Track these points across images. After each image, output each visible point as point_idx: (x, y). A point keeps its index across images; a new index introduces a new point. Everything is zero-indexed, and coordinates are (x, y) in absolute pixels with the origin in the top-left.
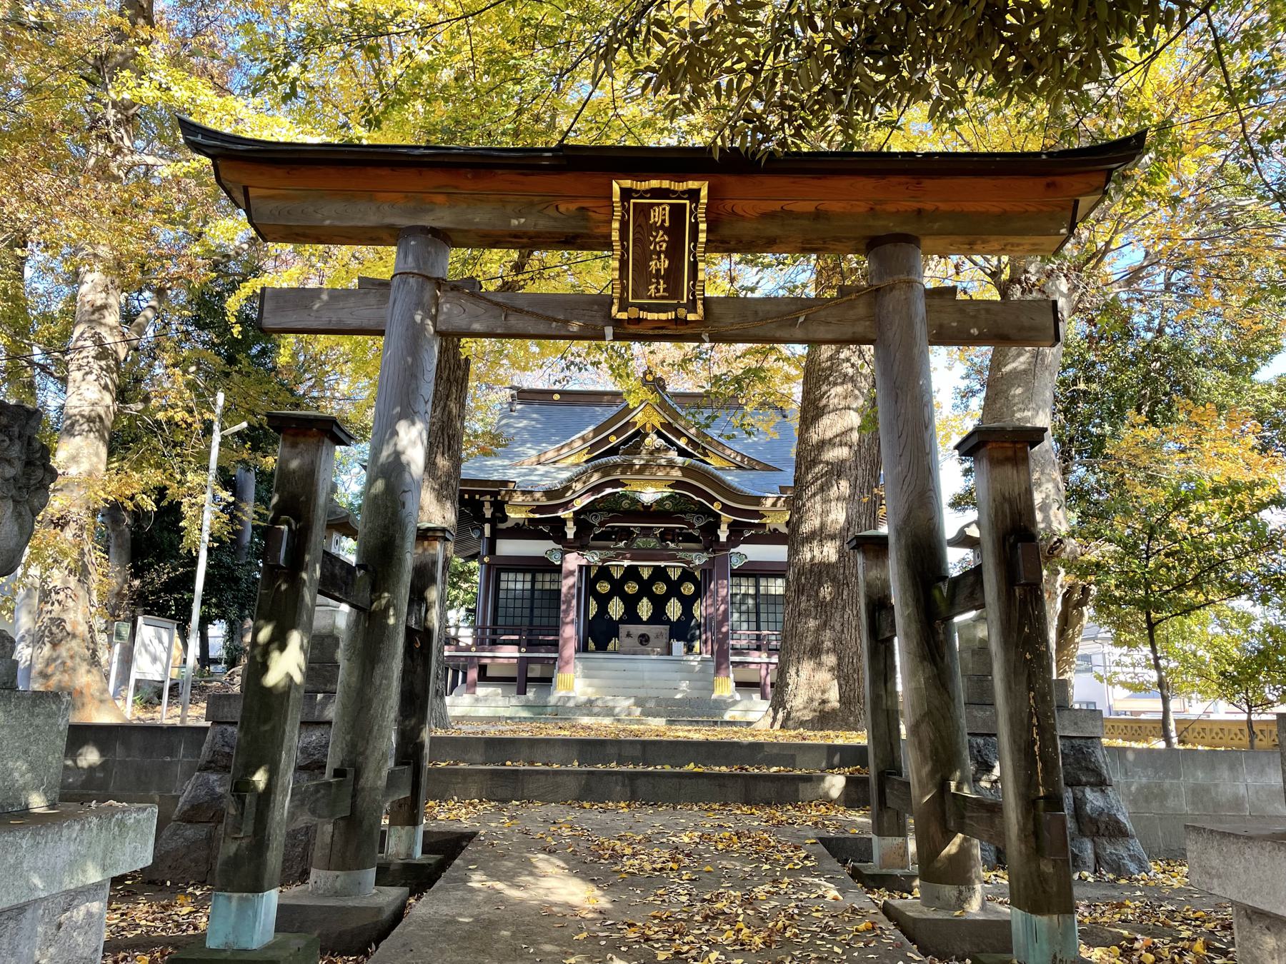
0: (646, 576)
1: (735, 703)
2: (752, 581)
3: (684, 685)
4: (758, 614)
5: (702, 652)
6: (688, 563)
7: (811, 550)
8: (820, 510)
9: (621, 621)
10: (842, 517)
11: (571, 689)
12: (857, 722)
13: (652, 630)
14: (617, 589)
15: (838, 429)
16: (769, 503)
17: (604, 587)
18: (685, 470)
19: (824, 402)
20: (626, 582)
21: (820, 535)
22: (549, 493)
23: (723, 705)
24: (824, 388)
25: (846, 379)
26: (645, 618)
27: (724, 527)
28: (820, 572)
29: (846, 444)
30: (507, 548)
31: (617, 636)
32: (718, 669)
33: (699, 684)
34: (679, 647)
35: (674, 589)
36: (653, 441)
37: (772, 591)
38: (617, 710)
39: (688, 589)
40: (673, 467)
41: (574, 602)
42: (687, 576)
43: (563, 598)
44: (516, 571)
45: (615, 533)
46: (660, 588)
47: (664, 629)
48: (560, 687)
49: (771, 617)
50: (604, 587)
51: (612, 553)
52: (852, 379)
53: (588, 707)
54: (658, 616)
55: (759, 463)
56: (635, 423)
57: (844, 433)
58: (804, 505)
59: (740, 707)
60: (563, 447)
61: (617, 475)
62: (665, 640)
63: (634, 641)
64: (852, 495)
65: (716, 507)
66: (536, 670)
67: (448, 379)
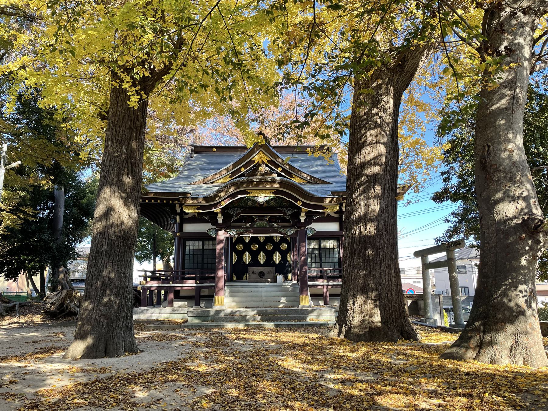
0: (262, 241)
1: (312, 311)
2: (317, 241)
3: (283, 300)
4: (320, 258)
5: (292, 281)
6: (284, 234)
7: (359, 228)
8: (363, 204)
9: (250, 265)
11: (222, 304)
12: (393, 335)
14: (247, 248)
15: (373, 154)
16: (328, 201)
17: (240, 247)
18: (281, 183)
19: (363, 140)
21: (365, 219)
22: (207, 199)
23: (305, 313)
25: (376, 125)
26: (262, 262)
27: (303, 214)
28: (365, 241)
29: (378, 164)
30: (189, 228)
31: (248, 272)
32: (301, 292)
33: (292, 298)
34: (280, 278)
35: (277, 247)
36: (263, 169)
38: (248, 317)
39: (284, 246)
40: (275, 182)
41: (223, 258)
42: (283, 240)
44: (194, 240)
46: (270, 247)
47: (271, 268)
48: (216, 304)
49: (328, 260)
50: (240, 247)
51: (243, 230)
52: (380, 126)
53: (231, 317)
54: (269, 262)
55: (319, 180)
56: (254, 161)
58: (353, 201)
59: (315, 313)
60: (216, 174)
61: (244, 188)
63: (256, 276)
64: (383, 194)
65: (299, 204)
66: (205, 292)
67: (130, 127)
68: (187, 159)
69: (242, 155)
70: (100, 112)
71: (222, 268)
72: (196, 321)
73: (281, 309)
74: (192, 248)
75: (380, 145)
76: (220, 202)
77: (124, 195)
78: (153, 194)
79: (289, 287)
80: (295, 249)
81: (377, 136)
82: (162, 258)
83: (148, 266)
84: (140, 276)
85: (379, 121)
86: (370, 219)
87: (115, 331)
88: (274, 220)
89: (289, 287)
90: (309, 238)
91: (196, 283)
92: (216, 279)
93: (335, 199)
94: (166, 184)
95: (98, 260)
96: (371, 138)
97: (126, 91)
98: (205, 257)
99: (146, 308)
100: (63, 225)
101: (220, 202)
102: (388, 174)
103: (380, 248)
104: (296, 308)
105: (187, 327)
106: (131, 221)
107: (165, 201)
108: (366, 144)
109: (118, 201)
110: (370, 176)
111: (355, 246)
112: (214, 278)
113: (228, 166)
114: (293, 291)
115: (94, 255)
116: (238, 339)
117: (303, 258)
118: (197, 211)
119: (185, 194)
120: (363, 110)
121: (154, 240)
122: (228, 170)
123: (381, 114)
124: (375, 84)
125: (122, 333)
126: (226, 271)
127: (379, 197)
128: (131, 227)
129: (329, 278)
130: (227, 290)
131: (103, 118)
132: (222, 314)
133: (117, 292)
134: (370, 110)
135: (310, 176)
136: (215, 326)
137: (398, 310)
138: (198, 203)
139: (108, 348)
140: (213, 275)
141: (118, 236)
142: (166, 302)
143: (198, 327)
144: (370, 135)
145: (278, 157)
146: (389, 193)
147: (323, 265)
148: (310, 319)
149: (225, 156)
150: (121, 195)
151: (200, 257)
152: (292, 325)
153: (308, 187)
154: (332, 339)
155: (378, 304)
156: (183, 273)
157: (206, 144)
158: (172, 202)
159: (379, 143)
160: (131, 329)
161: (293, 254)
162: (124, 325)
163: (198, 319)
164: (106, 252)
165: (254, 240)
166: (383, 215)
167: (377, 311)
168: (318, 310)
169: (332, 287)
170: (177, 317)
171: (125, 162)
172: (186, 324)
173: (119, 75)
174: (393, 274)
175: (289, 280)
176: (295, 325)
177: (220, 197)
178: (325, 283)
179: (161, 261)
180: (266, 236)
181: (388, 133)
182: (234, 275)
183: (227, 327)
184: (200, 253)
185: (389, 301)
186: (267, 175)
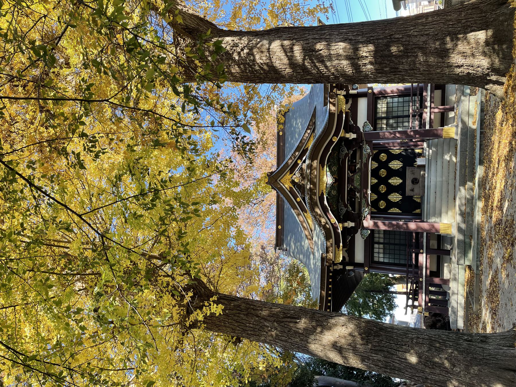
0: (376, 181)
1: (463, 122)
2: (379, 122)
3: (447, 157)
7: (365, 65)
9: (403, 194)
10: (342, 45)
11: (450, 226)
12: (504, 14)
13: (409, 177)
14: (384, 197)
15: (282, 55)
16: (333, 108)
17: (382, 204)
19: (265, 67)
20: (380, 192)
22: (328, 237)
23: (466, 132)
24: (257, 68)
25: (251, 53)
26: (401, 181)
27: (348, 135)
30: (359, 257)
32: (438, 136)
33: (445, 147)
34: (420, 161)
35: (384, 165)
36: (297, 177)
37: (385, 109)
38: (468, 196)
40: (311, 165)
41: (394, 222)
42: (376, 158)
43: (391, 229)
44: (373, 253)
45: (351, 198)
46: (383, 173)
50: (382, 204)
51: (363, 201)
52: (251, 49)
54: (401, 173)
56: (290, 188)
57: (285, 52)
58: (333, 74)
59: (466, 119)
60: (304, 227)
61: (316, 198)
62: (416, 170)
64: (326, 40)
65: (336, 140)
66: (434, 244)
67: (247, 315)
68: (289, 255)
69: (286, 201)
70: (233, 343)
71: (406, 224)
72: (470, 255)
73: (458, 159)
74: (381, 255)
75: (271, 47)
76: (332, 224)
77: (319, 330)
78: (322, 292)
79: (431, 151)
80: (387, 145)
81: (262, 52)
82: (392, 285)
83: (400, 301)
84: (412, 312)
85: (246, 51)
86: (354, 53)
87: (488, 357)
88: (353, 167)
89: (431, 151)
90: (375, 129)
91: (423, 253)
92: (420, 231)
93: (331, 100)
94: (313, 278)
95: (395, 367)
96: (264, 58)
97: (205, 317)
98: (392, 241)
99: (450, 309)
100: (354, 381)
101: (332, 224)
102: (303, 36)
103: (391, 38)
104: (459, 142)
105: (477, 267)
106: (349, 325)
107: (330, 280)
108: (270, 64)
109: (325, 337)
110: (304, 57)
111: (387, 69)
112: (417, 234)
113: (295, 214)
114: (436, 146)
115: (388, 371)
116: (501, 208)
117: (398, 135)
118: (341, 248)
119: (323, 259)
120: (235, 70)
121: (372, 291)
122: (298, 215)
123: (239, 50)
124: (210, 58)
125: (491, 347)
126: (410, 220)
127: (328, 45)
128: (356, 325)
129: (422, 106)
130: (432, 220)
131: (239, 340)
132: (463, 226)
133: (437, 350)
134: (234, 61)
135: (307, 129)
136: (478, 234)
137: (470, 11)
138: (332, 246)
139: (510, 367)
140: (414, 234)
141: (367, 342)
142: (443, 286)
143: (479, 254)
144: (260, 59)
145: (287, 163)
146: (325, 33)
147: (406, 113)
148: (473, 124)
149: (286, 216)
150: (319, 333)
151: (392, 247)
152: (481, 145)
153: (318, 132)
154: (506, 92)
155: (462, 36)
156: (411, 266)
157: (273, 234)
158: (331, 272)
159: (269, 49)
160: (484, 337)
161: (392, 148)
162: (480, 345)
163: (468, 253)
164: (385, 357)
165: (375, 189)
166: (350, 37)
167: (472, 36)
168: (463, 116)
169: (433, 102)
170: (463, 275)
171: (282, 324)
172: (474, 268)
173: (191, 323)
174: (424, 20)
175: (423, 151)
176: (481, 141)
177: (327, 223)
178: (428, 110)
179: (394, 286)
180: (371, 176)
181: (259, 40)
182: (414, 212)
183: (480, 220)
184: (387, 246)
185: (459, 23)
186: (303, 174)
